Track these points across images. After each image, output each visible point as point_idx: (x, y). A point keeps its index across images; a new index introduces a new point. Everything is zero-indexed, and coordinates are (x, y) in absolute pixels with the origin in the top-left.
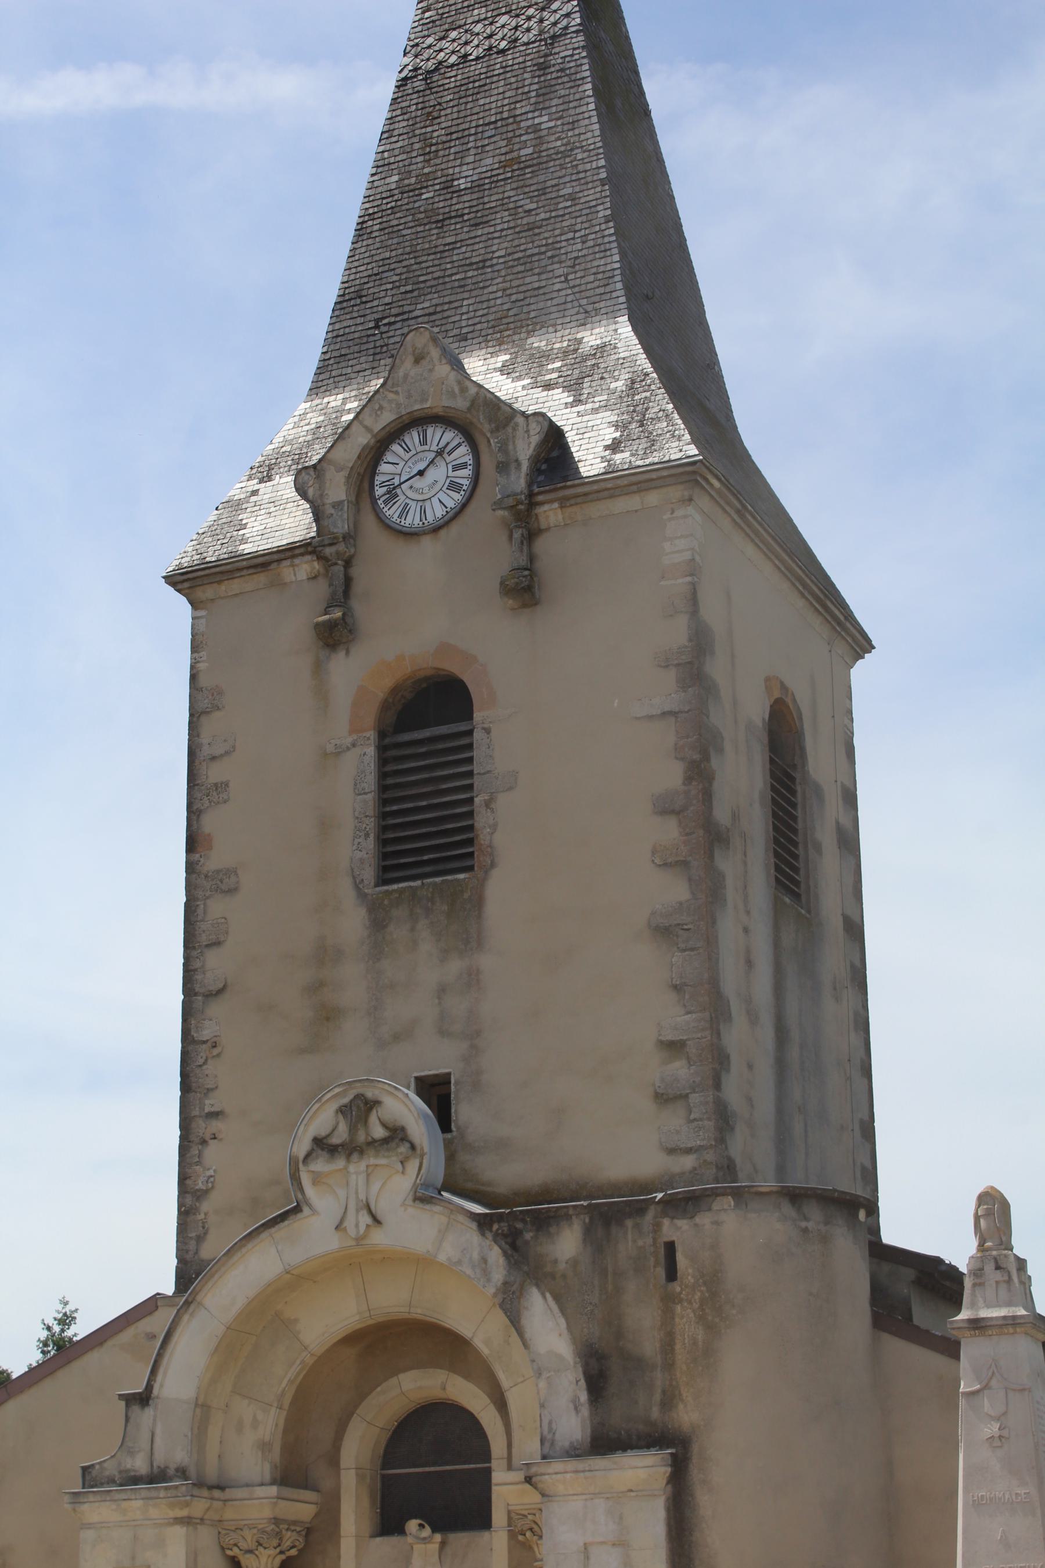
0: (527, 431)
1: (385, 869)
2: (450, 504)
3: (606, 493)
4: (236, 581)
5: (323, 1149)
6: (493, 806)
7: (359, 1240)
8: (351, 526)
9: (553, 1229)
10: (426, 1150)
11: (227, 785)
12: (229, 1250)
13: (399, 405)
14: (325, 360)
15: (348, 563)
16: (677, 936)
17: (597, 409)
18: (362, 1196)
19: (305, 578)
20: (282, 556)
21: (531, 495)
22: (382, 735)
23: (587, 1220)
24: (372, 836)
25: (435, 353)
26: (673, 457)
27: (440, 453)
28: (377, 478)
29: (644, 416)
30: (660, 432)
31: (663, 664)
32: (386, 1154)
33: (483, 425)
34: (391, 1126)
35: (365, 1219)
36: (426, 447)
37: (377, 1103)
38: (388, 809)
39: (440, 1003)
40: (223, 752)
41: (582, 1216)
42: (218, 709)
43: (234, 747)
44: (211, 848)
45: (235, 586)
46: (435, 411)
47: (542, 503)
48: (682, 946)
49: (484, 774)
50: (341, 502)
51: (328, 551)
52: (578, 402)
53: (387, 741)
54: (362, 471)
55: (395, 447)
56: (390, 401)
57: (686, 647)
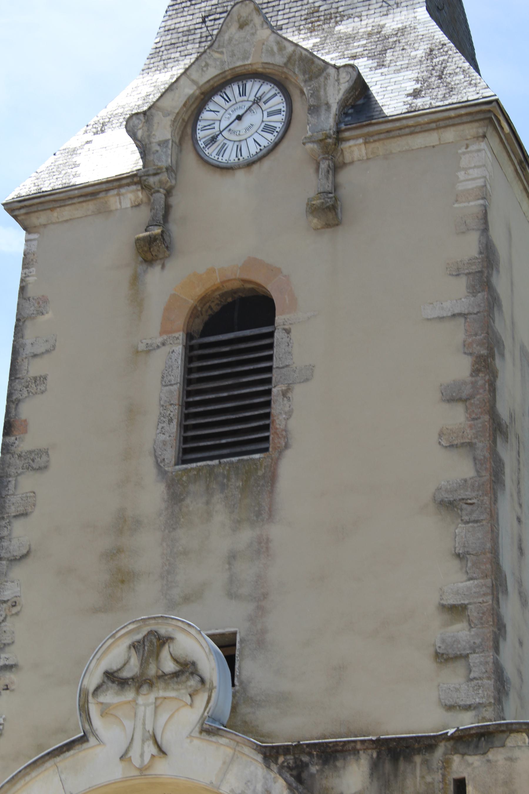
0: (338, 80)
1: (185, 451)
2: (264, 143)
3: (407, 130)
4: (67, 208)
5: (113, 682)
6: (289, 395)
7: (143, 770)
8: (174, 162)
9: (339, 764)
10: (215, 683)
11: (45, 378)
12: (13, 778)
13: (223, 63)
14: (156, 48)
15: (168, 193)
16: (461, 510)
17: (399, 70)
18: (149, 727)
19: (129, 205)
20: (110, 185)
21: (338, 132)
22: (189, 336)
23: (375, 755)
24: (175, 422)
25: (257, 20)
26: (470, 98)
27: (257, 101)
28: (199, 123)
29: (442, 72)
30: (457, 82)
31: (454, 273)
32: (176, 687)
33: (298, 78)
34: (182, 661)
35: (151, 749)
36: (245, 98)
37: (169, 639)
38: (191, 399)
39: (230, 569)
40: (43, 350)
41: (370, 751)
42: (43, 314)
43: (54, 347)
44: (26, 432)
45: (67, 212)
46: (255, 67)
47: (347, 140)
48: (466, 518)
49: (283, 368)
50: (166, 141)
51: (152, 180)
52: (381, 65)
53: (194, 342)
54: (186, 118)
55: (217, 99)
56: (215, 60)
57: (477, 258)
